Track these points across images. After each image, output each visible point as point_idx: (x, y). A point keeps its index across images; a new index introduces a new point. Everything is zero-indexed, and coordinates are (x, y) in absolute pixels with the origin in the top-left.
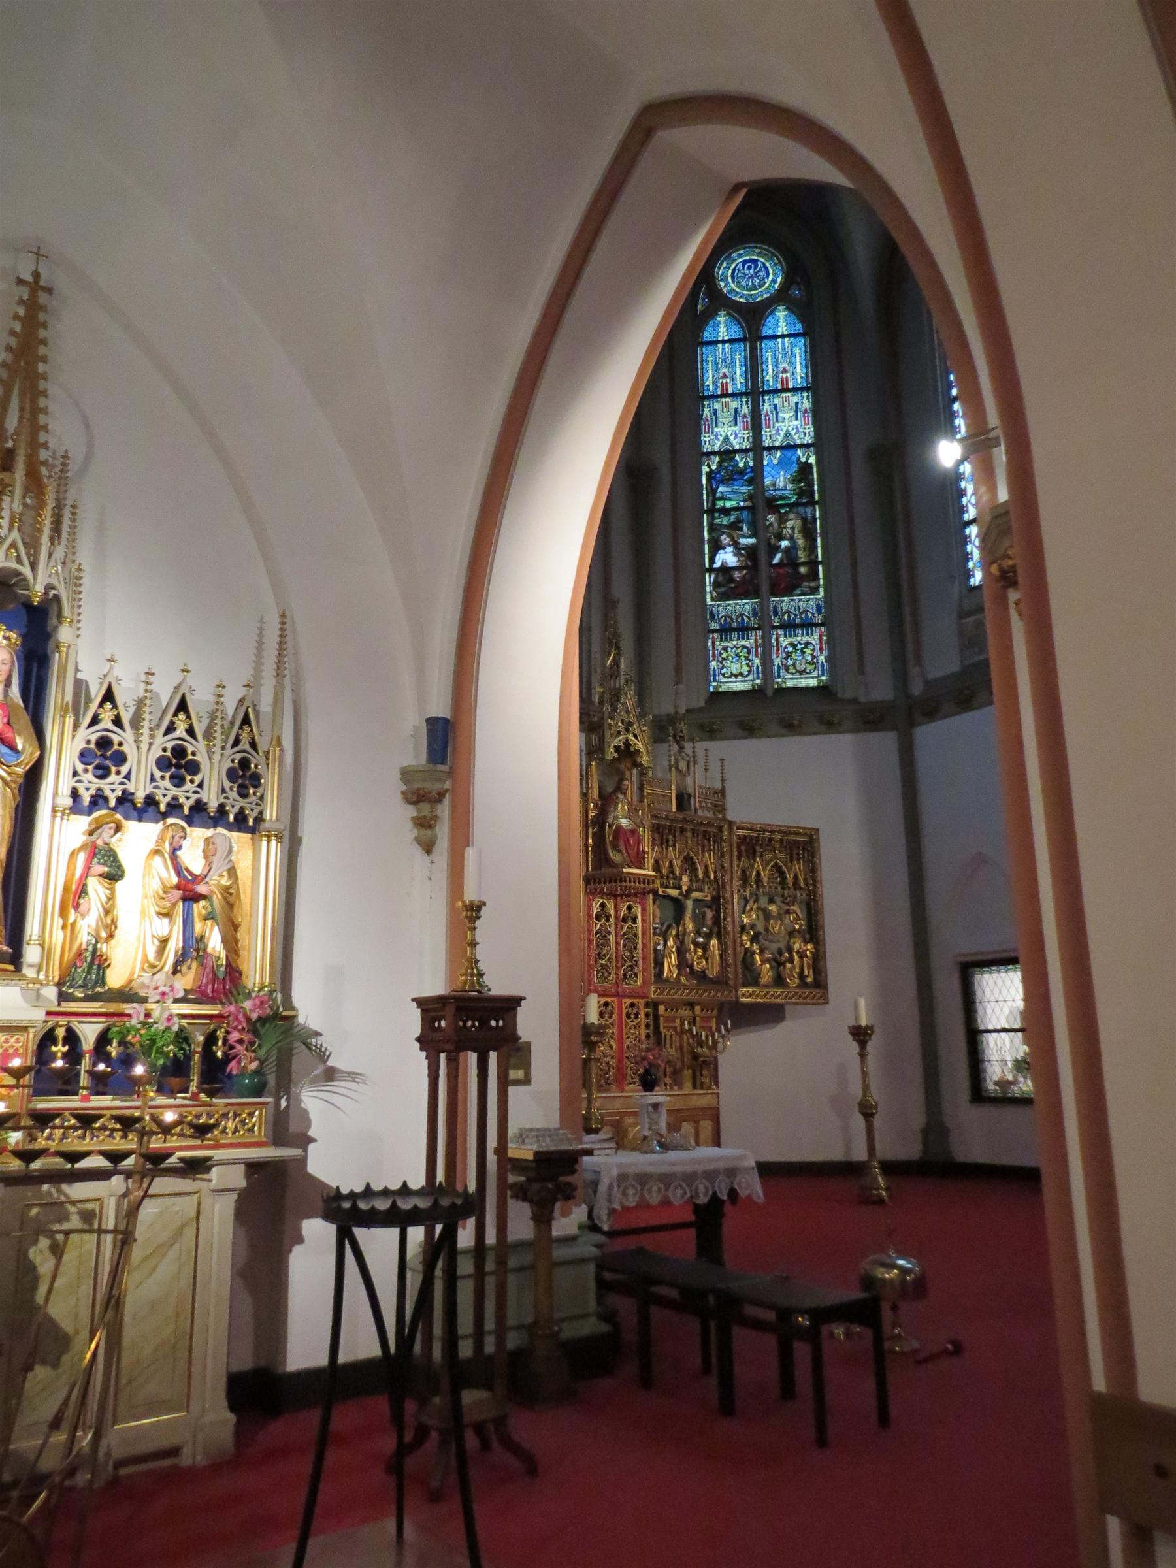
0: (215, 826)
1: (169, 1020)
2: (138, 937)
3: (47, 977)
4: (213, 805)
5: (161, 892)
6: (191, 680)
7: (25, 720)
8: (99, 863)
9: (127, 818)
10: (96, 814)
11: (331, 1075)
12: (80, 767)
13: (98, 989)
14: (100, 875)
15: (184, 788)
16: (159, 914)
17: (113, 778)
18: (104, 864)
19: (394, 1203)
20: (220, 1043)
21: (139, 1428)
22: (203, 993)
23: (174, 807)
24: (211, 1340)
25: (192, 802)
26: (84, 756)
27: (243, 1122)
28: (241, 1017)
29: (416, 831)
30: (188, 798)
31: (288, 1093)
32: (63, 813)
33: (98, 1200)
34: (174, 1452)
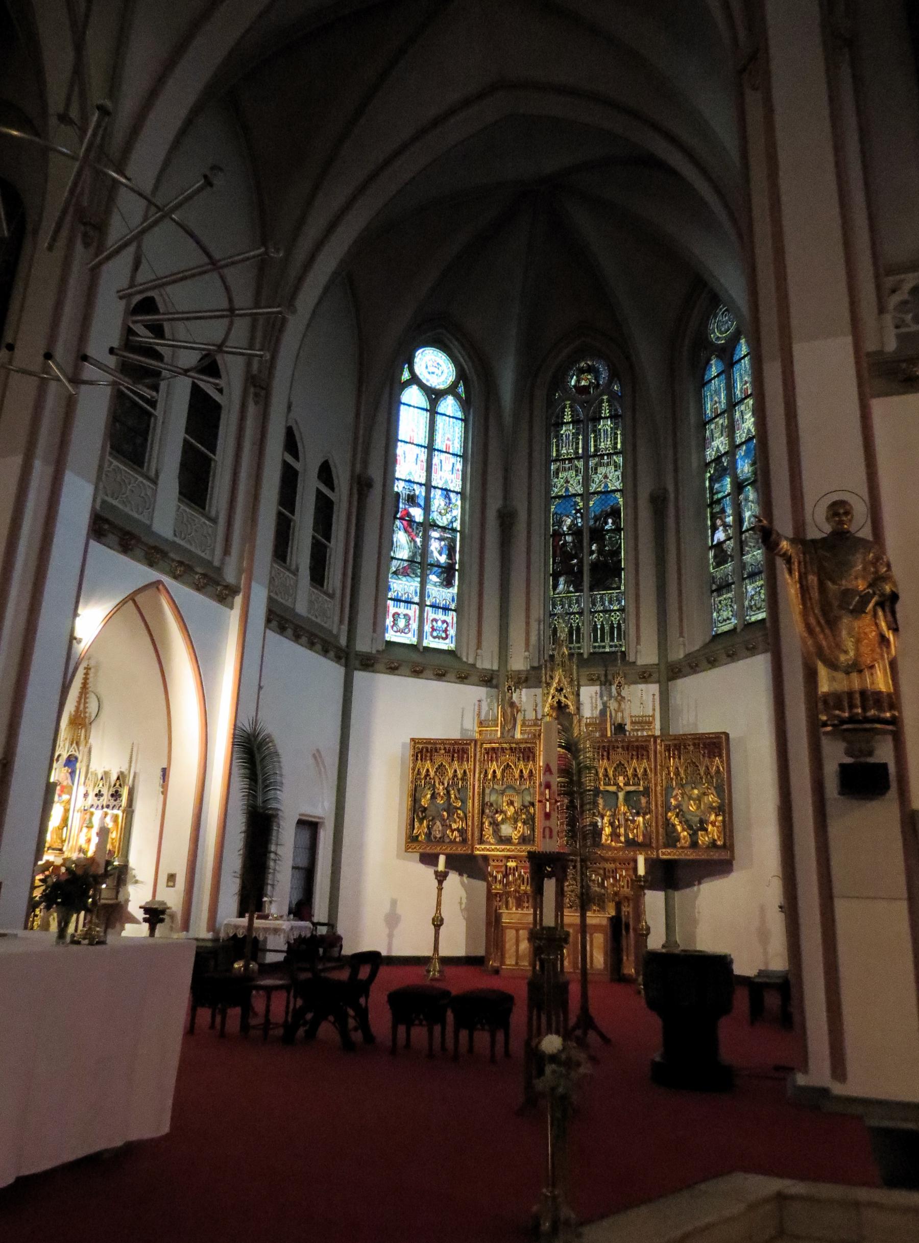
11: (136, 882)
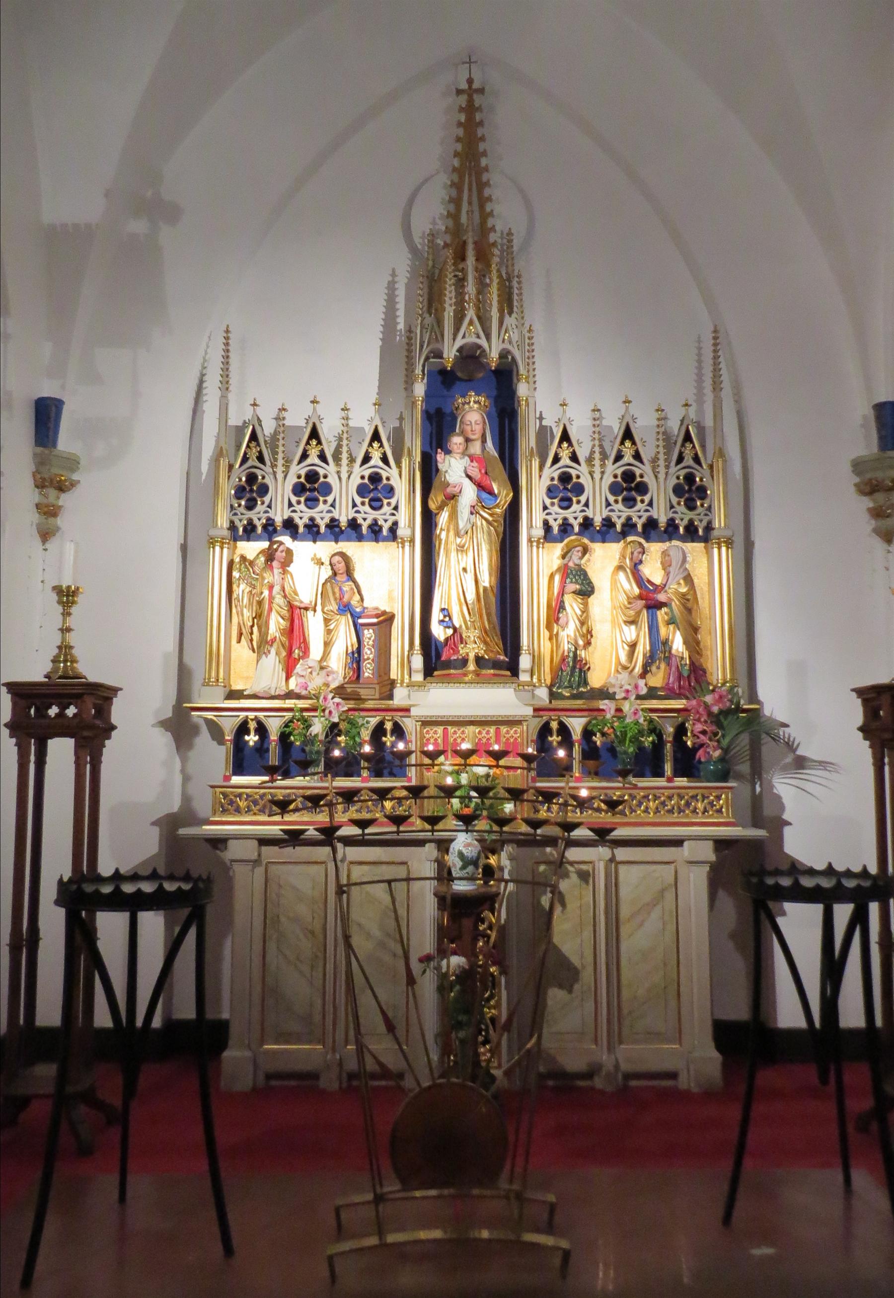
0: (670, 539)
1: (635, 714)
2: (612, 644)
3: (539, 680)
4: (663, 521)
5: (626, 603)
6: (633, 409)
7: (499, 470)
8: (571, 582)
9: (593, 540)
10: (566, 541)
11: (801, 763)
12: (548, 502)
13: (582, 689)
14: (573, 592)
15: (636, 508)
16: (625, 622)
17: (575, 507)
18: (576, 582)
19: (161, 886)
20: (689, 734)
21: (639, 1054)
22: (671, 690)
23: (629, 527)
24: (695, 991)
25: (644, 520)
26: (551, 491)
27: (711, 804)
28: (701, 710)
29: (873, 522)
30: (640, 517)
31: (760, 779)
32: (538, 542)
33: (591, 862)
34: (673, 1076)
